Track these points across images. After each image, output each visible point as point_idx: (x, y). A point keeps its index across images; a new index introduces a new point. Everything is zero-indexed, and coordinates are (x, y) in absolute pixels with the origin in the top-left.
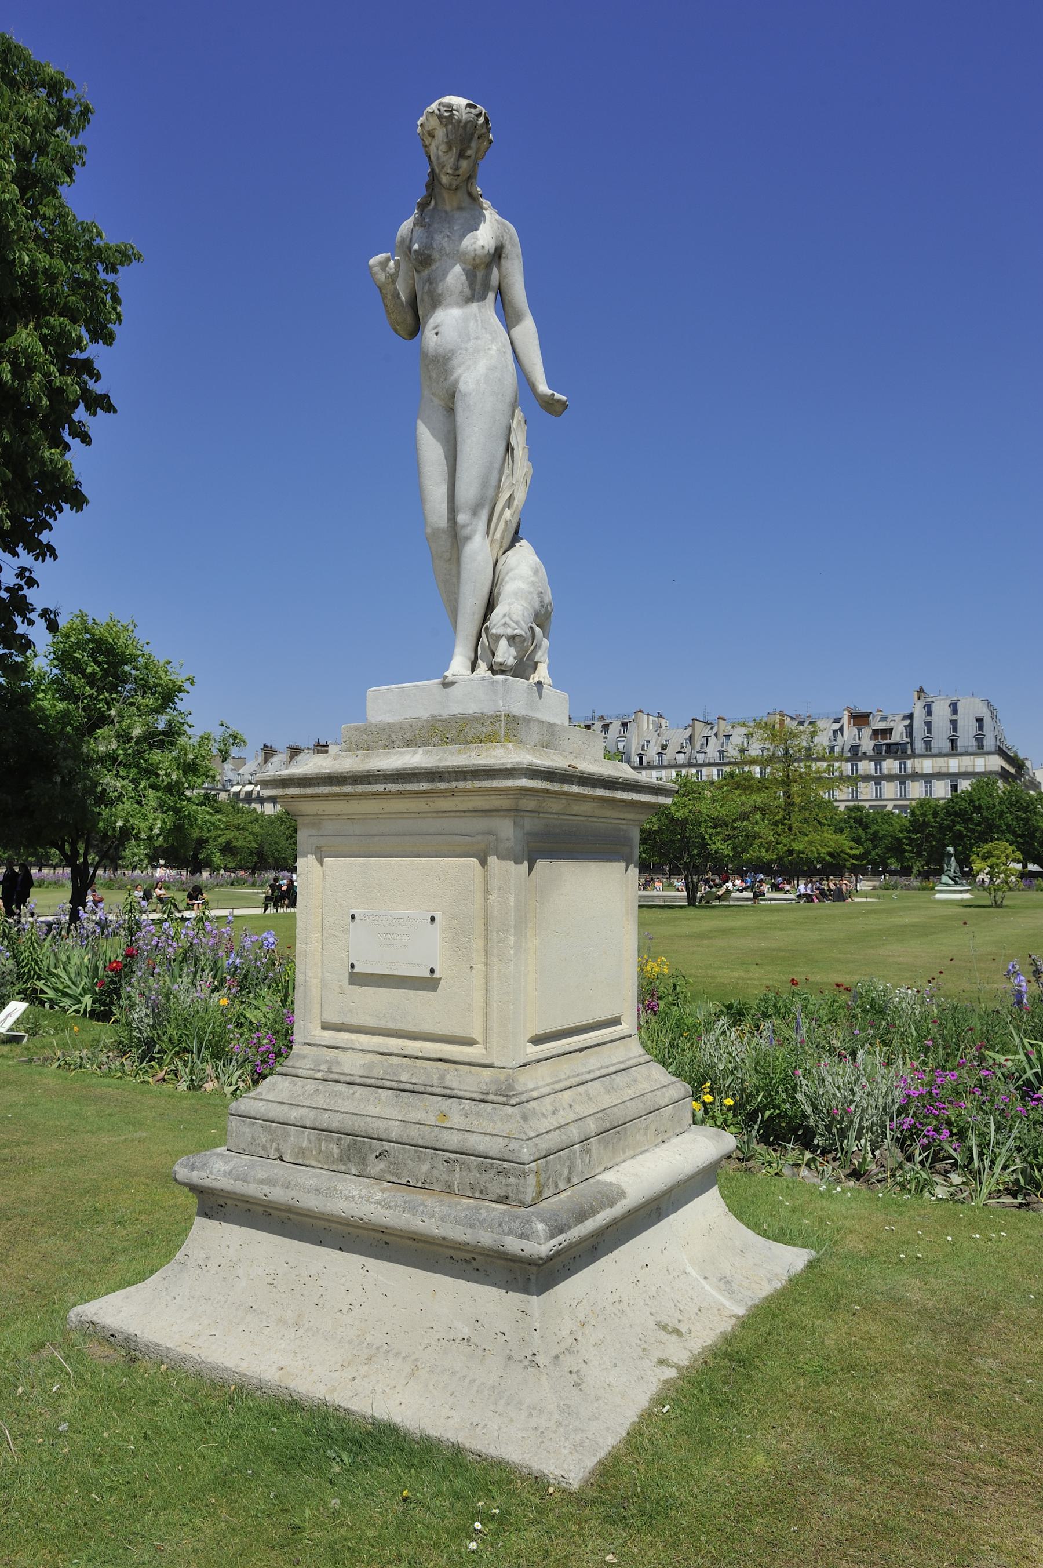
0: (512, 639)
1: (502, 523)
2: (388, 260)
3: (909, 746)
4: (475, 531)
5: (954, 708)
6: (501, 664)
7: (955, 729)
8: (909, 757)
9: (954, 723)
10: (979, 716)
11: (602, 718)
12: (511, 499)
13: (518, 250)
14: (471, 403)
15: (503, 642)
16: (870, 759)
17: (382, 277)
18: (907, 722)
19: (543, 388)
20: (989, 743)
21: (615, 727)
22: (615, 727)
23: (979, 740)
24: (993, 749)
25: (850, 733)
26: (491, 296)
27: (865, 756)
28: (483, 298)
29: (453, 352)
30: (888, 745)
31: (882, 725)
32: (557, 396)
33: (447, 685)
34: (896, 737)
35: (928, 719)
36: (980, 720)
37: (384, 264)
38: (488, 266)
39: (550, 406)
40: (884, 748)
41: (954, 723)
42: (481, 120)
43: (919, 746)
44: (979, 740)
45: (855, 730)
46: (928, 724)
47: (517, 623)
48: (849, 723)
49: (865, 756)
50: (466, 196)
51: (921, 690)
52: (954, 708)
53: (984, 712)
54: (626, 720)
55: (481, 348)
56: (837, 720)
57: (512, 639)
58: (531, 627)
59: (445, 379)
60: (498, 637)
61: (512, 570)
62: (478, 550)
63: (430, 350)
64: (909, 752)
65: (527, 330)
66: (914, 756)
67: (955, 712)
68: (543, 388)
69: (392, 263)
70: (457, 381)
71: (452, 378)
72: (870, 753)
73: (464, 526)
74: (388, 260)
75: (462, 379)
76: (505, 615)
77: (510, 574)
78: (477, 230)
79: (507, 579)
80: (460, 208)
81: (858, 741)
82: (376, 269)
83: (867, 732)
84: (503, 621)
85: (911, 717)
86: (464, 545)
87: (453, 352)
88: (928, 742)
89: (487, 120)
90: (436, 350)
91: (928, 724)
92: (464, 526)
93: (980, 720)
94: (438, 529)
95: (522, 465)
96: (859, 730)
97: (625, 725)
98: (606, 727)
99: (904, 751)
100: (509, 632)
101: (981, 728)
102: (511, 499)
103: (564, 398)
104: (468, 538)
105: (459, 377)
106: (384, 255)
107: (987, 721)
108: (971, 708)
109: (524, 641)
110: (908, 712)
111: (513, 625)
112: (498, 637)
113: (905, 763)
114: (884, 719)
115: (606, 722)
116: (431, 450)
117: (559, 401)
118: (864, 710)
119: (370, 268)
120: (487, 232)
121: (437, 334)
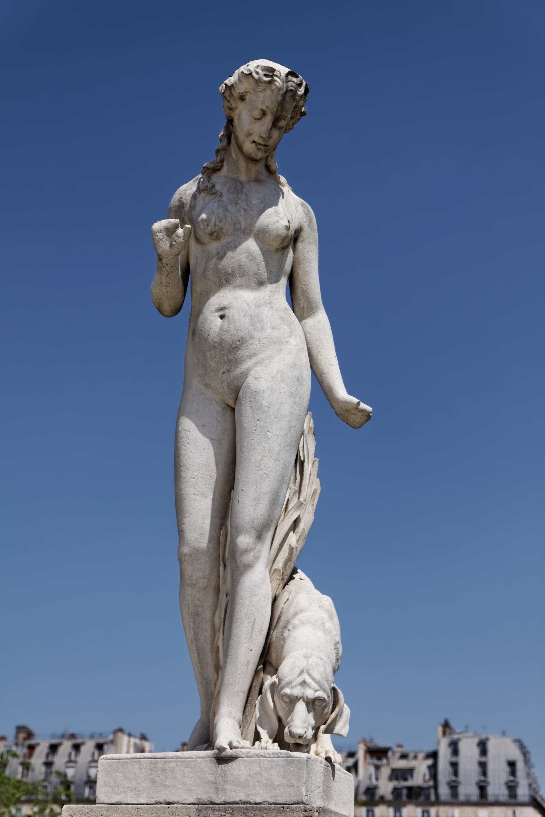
0: (312, 704)
1: (286, 547)
2: (176, 227)
3: (432, 791)
4: (257, 558)
5: (483, 747)
6: (300, 737)
7: (484, 773)
8: (433, 804)
9: (483, 766)
10: (511, 758)
11: (73, 736)
12: (296, 523)
13: (315, 235)
14: (265, 403)
15: (301, 707)
16: (389, 804)
17: (164, 245)
18: (430, 762)
19: (341, 392)
20: (523, 792)
21: (88, 748)
22: (88, 748)
23: (512, 788)
24: (526, 799)
25: (366, 770)
26: (284, 282)
27: (382, 800)
28: (277, 281)
29: (242, 341)
30: (410, 789)
31: (402, 764)
32: (363, 406)
33: (222, 759)
34: (420, 778)
35: (454, 759)
36: (512, 764)
37: (170, 231)
38: (284, 249)
39: (344, 413)
40: (405, 792)
41: (483, 766)
42: (301, 91)
43: (444, 791)
44: (512, 788)
45: (372, 770)
46: (454, 765)
47: (318, 683)
48: (365, 758)
49: (382, 800)
50: (264, 168)
51: (446, 726)
52: (483, 747)
53: (516, 754)
54: (101, 741)
55: (280, 343)
56: (351, 755)
57: (312, 704)
58: (334, 689)
59: (228, 371)
60: (292, 701)
61: (302, 611)
62: (257, 585)
63: (212, 334)
64: (433, 798)
65: (320, 322)
66: (438, 802)
67: (484, 751)
68: (341, 392)
69: (180, 231)
70: (245, 375)
71: (239, 371)
72: (389, 797)
73: (246, 551)
74: (176, 227)
75: (253, 373)
76: (302, 672)
77: (300, 617)
78: (275, 203)
79: (295, 621)
80: (258, 181)
81: (374, 781)
82: (160, 235)
83: (385, 772)
84: (300, 679)
85: (434, 755)
86: (243, 573)
87: (242, 341)
88: (454, 787)
89: (307, 90)
90: (220, 336)
91: (454, 765)
92: (246, 551)
93: (512, 764)
94: (197, 550)
95: (312, 483)
96: (377, 768)
97: (100, 747)
98: (77, 747)
99: (428, 797)
100: (310, 694)
101: (513, 773)
102: (296, 523)
103: (369, 409)
104: (248, 567)
105: (248, 370)
106: (173, 221)
107: (520, 765)
108: (502, 749)
109: (325, 707)
110: (430, 748)
111: (314, 685)
112: (292, 701)
113: (428, 812)
114: (404, 756)
115: (78, 741)
116: (199, 453)
117: (363, 411)
118: (381, 743)
119: (152, 233)
120: (289, 210)
121: (222, 317)
